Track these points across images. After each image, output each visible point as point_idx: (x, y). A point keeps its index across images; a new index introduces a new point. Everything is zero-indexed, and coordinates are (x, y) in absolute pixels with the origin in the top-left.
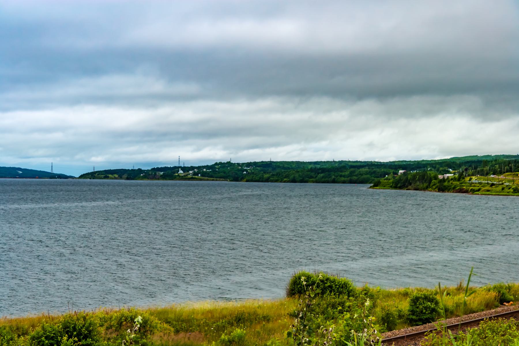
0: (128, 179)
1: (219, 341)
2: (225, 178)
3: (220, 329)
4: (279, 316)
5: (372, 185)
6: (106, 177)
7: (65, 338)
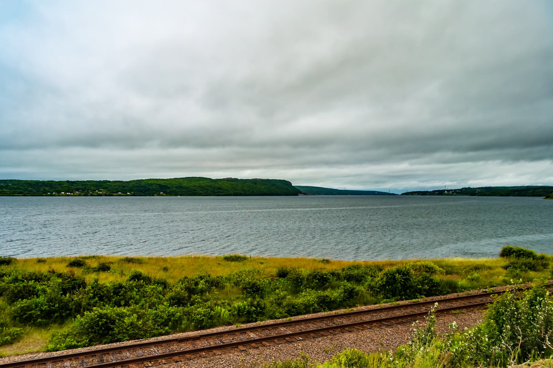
0: (422, 195)
1: (467, 279)
2: (467, 194)
3: (467, 272)
4: (497, 267)
5: (545, 197)
6: (412, 195)
7: (397, 275)
